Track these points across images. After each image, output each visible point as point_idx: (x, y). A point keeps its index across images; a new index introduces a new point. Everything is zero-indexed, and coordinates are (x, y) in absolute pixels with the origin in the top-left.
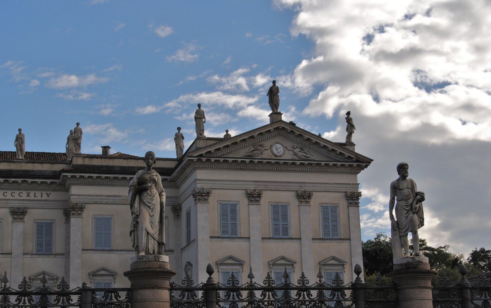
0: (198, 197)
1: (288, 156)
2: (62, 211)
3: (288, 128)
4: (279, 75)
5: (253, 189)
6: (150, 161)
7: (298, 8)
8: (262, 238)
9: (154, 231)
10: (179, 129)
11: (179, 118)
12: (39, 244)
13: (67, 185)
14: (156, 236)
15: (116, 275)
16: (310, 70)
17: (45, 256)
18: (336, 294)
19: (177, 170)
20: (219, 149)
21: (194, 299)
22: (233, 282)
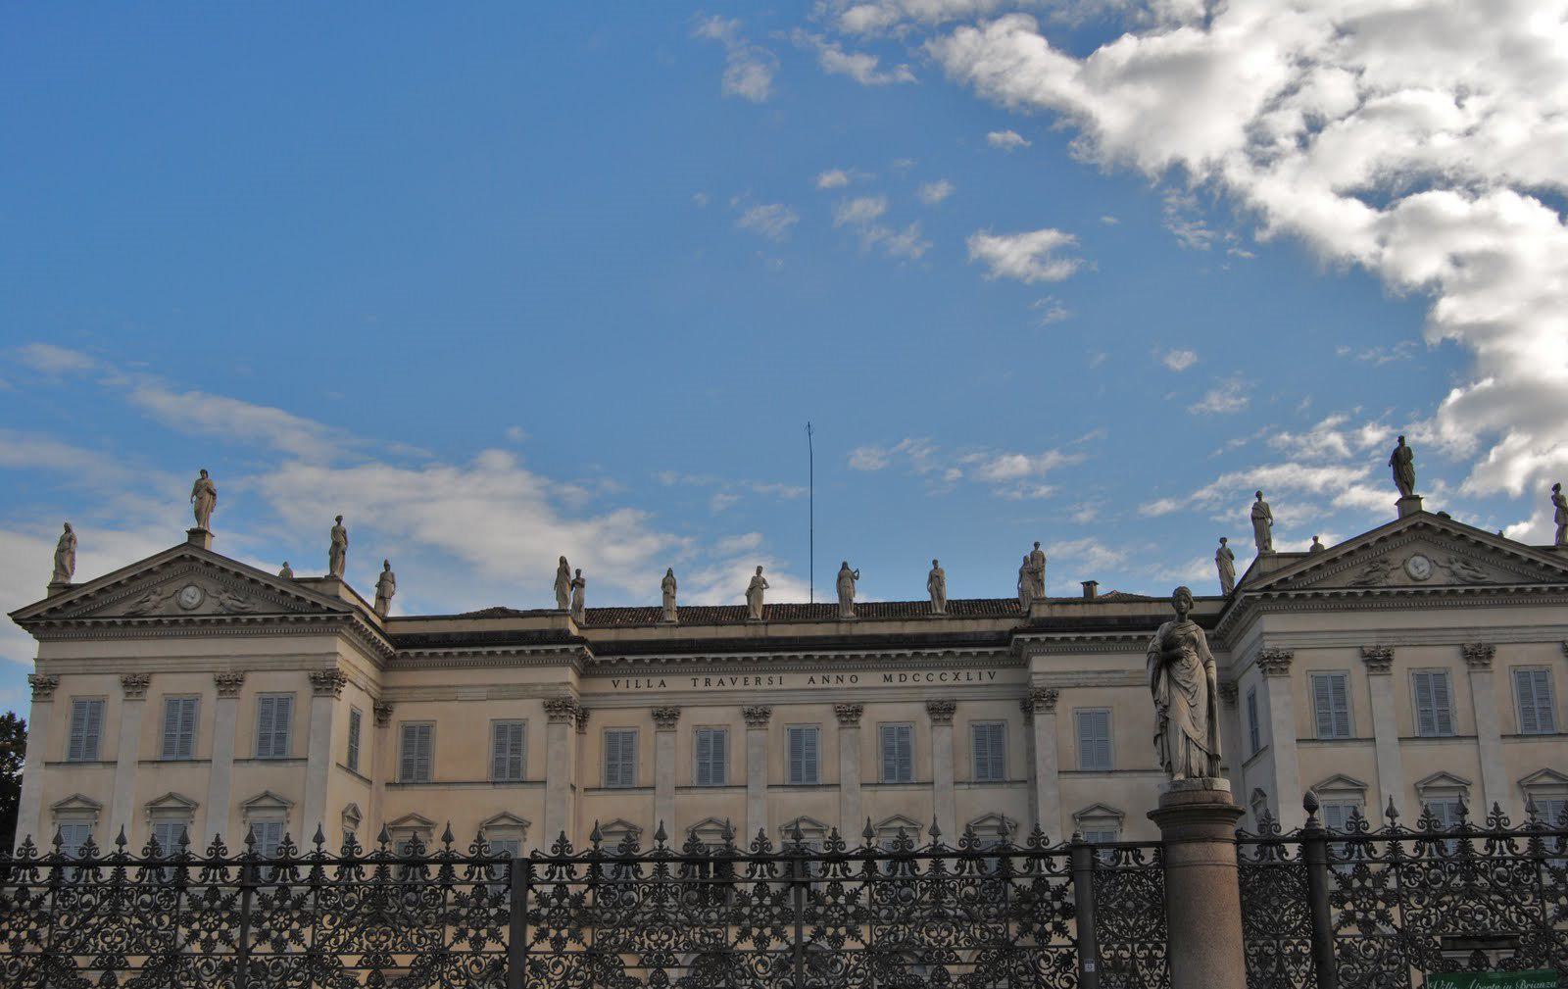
0: (1268, 666)
1: (1440, 578)
2: (1018, 702)
3: (1436, 525)
4: (1408, 422)
5: (1374, 645)
6: (1183, 604)
7: (1435, 290)
8: (1400, 739)
9: (1199, 734)
10: (1223, 540)
11: (1220, 518)
12: (981, 765)
13: (1024, 656)
14: (1204, 743)
15: (1123, 817)
16: (1464, 408)
17: (993, 786)
18: (1356, 848)
19: (1226, 617)
20: (1302, 574)
21: (1282, 859)
22: (1498, 820)
